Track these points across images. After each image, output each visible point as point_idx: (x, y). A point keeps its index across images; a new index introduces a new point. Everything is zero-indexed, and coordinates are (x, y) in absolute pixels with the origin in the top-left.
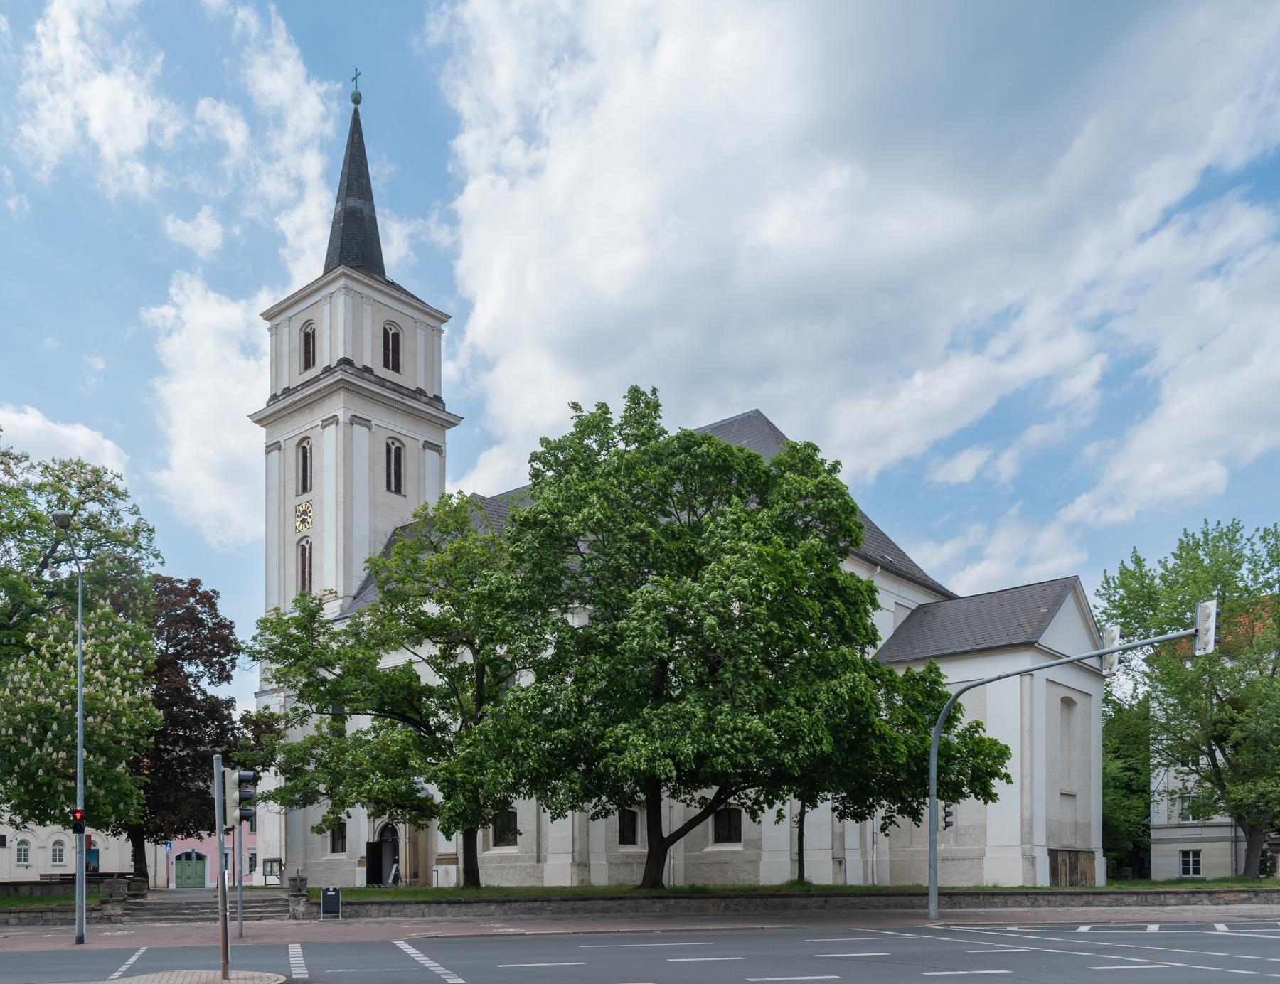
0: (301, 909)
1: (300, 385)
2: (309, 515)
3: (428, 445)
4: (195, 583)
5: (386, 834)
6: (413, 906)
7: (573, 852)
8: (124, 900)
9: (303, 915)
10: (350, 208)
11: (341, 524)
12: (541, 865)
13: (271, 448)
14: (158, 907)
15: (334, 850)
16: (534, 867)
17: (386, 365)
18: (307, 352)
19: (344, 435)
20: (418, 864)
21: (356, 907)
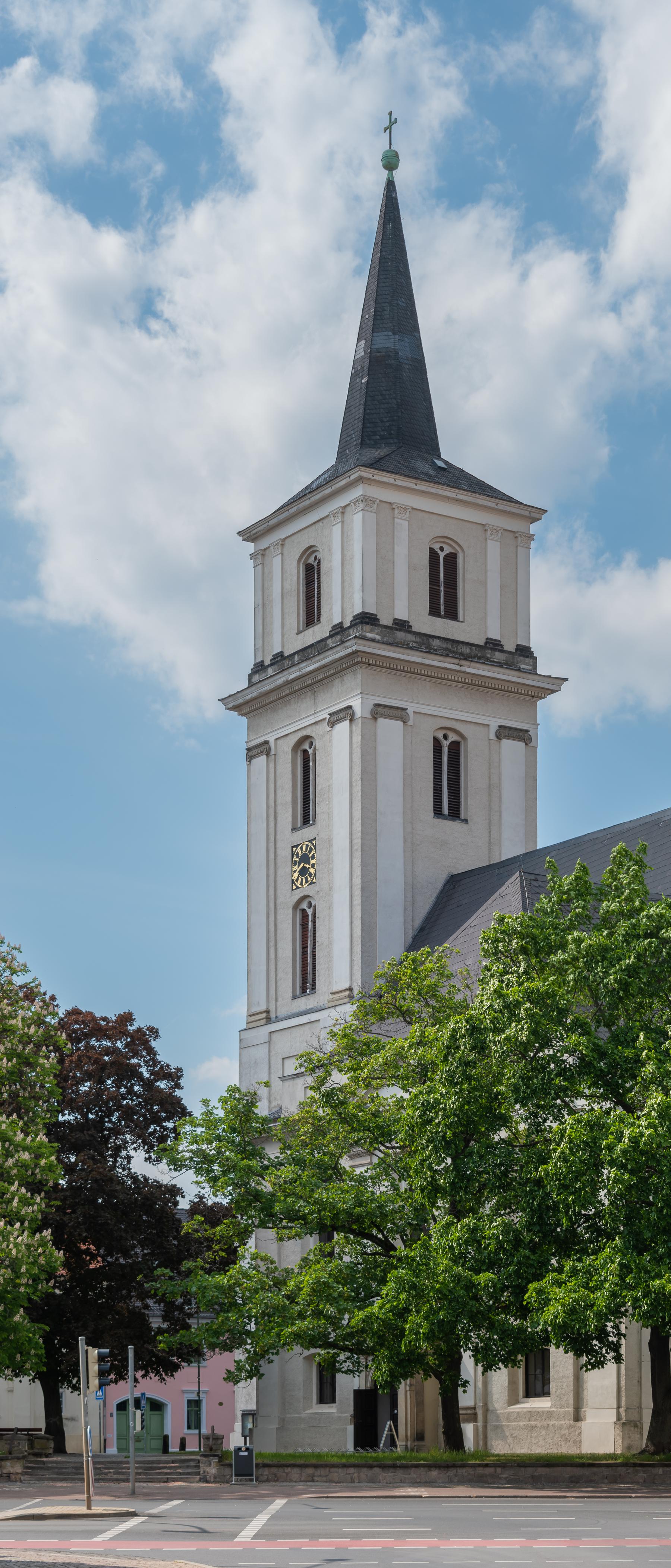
0: (213, 1470)
1: (297, 652)
2: (313, 862)
3: (504, 732)
4: (127, 1018)
6: (340, 1470)
7: (619, 1407)
8: (24, 1457)
9: (215, 1478)
11: (358, 881)
12: (578, 1424)
13: (255, 751)
14: (59, 1466)
15: (322, 1400)
16: (570, 1427)
17: (434, 611)
19: (363, 737)
20: (423, 1422)
21: (274, 1470)
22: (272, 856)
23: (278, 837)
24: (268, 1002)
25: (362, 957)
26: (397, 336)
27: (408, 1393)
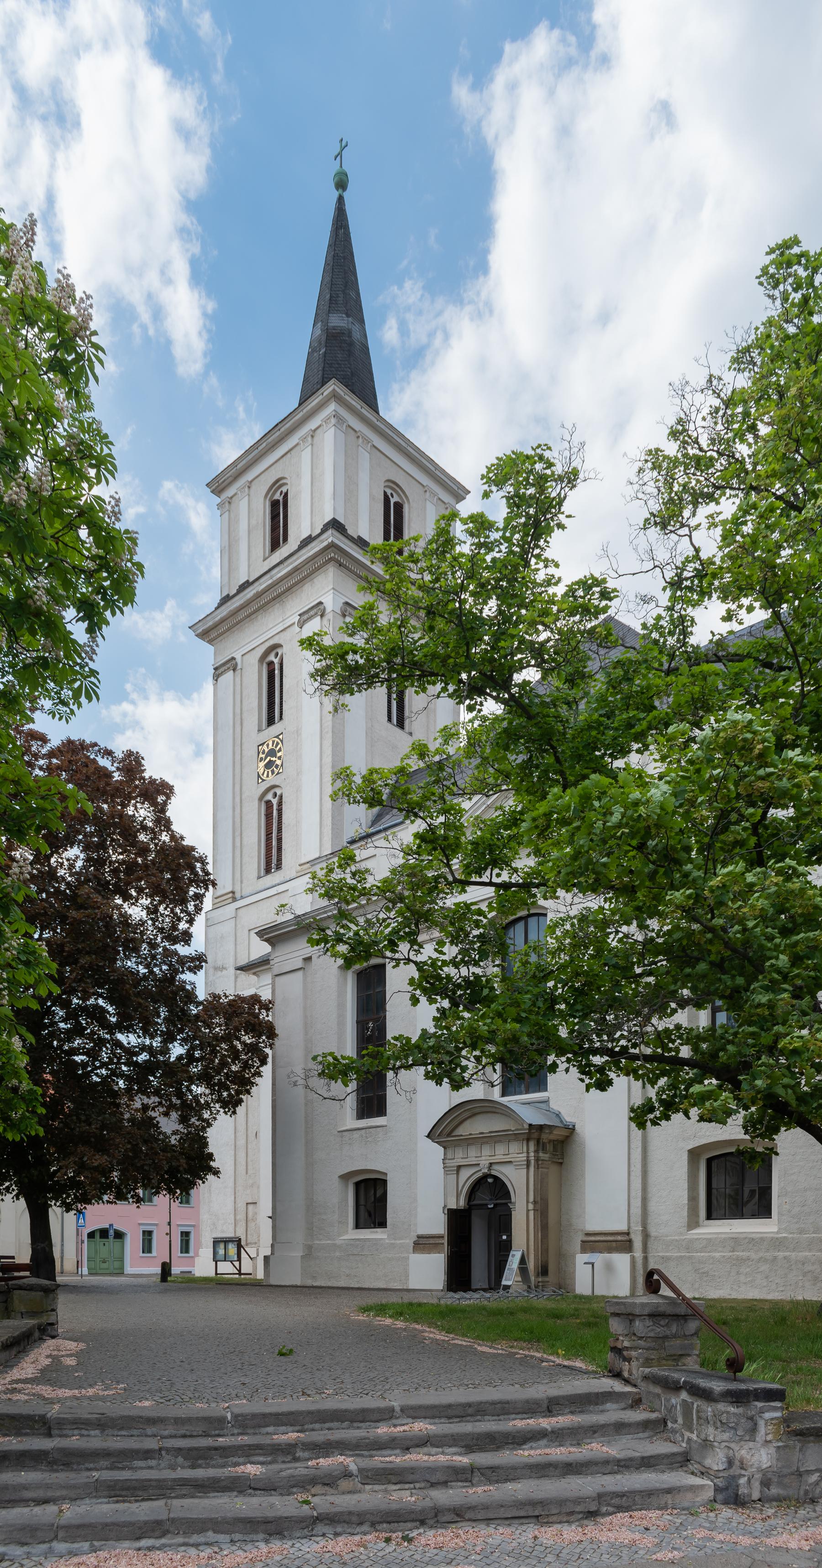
2: (279, 754)
5: (479, 1194)
9: (766, 1483)
10: (334, 328)
13: (222, 669)
18: (274, 528)
22: (238, 757)
23: (244, 740)
24: (233, 884)
25: (333, 829)
26: (350, 319)
27: (531, 1213)
